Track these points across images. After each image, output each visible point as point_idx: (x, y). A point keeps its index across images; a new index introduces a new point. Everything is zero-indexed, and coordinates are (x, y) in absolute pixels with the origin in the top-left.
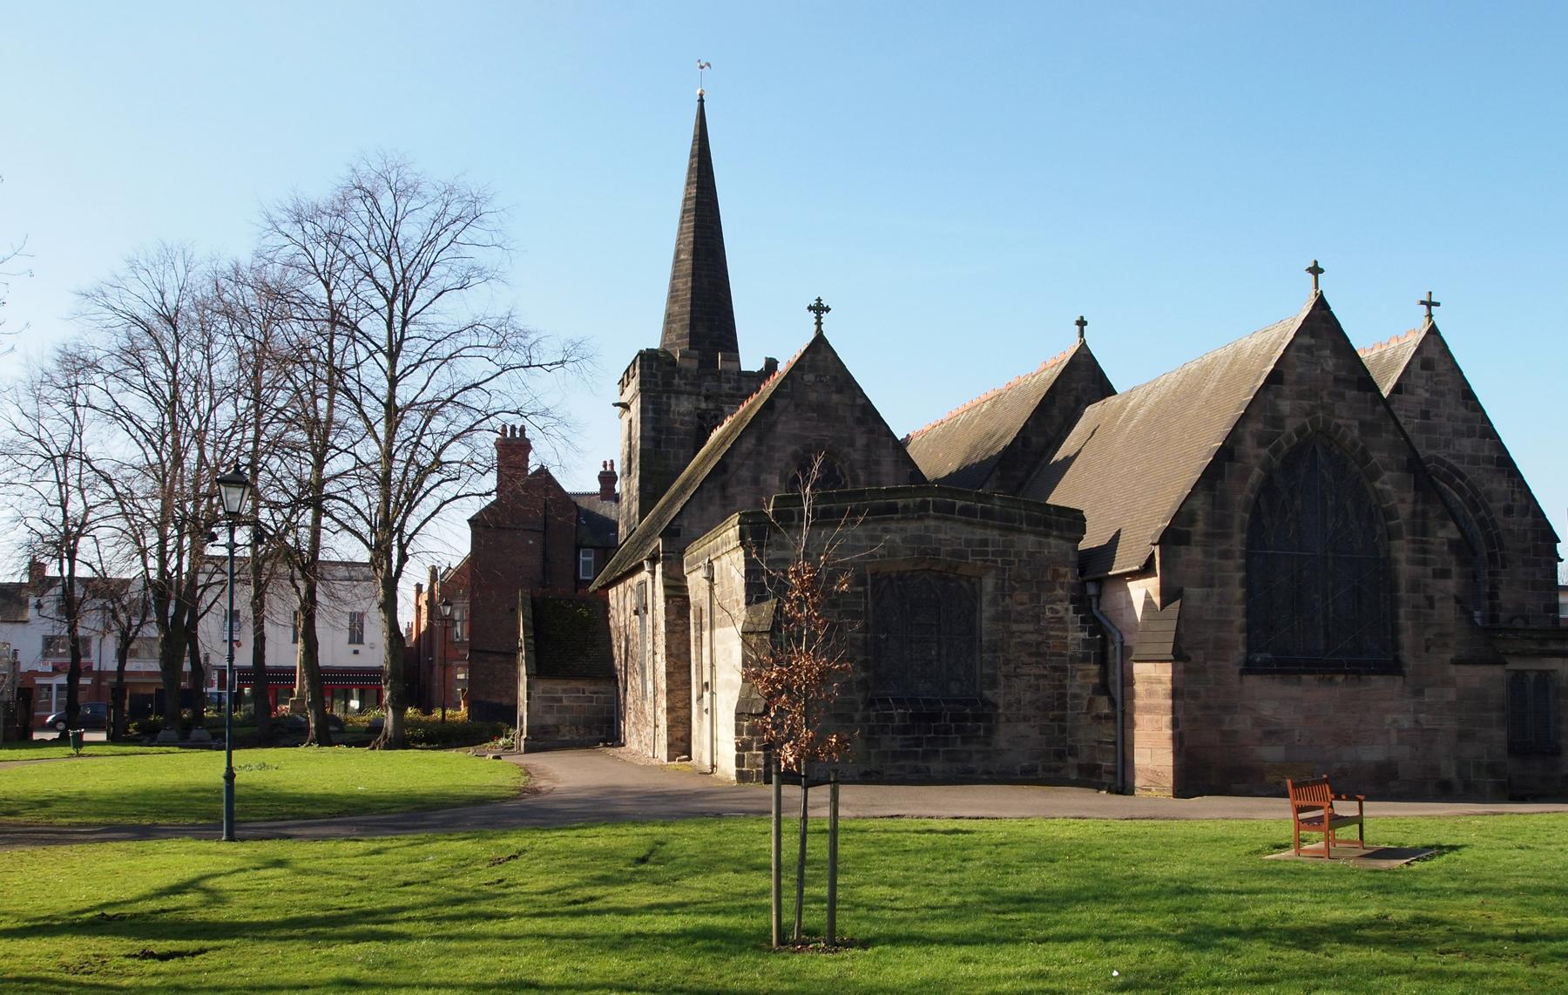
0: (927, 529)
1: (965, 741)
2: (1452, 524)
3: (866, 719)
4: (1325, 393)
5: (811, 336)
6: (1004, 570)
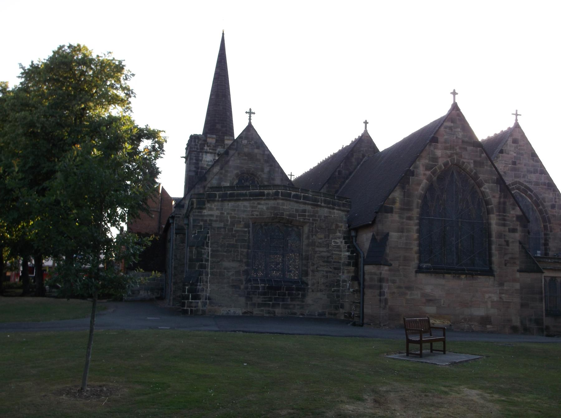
0: (278, 204)
1: (292, 300)
2: (518, 208)
3: (246, 288)
4: (457, 148)
5: (247, 124)
6: (313, 224)
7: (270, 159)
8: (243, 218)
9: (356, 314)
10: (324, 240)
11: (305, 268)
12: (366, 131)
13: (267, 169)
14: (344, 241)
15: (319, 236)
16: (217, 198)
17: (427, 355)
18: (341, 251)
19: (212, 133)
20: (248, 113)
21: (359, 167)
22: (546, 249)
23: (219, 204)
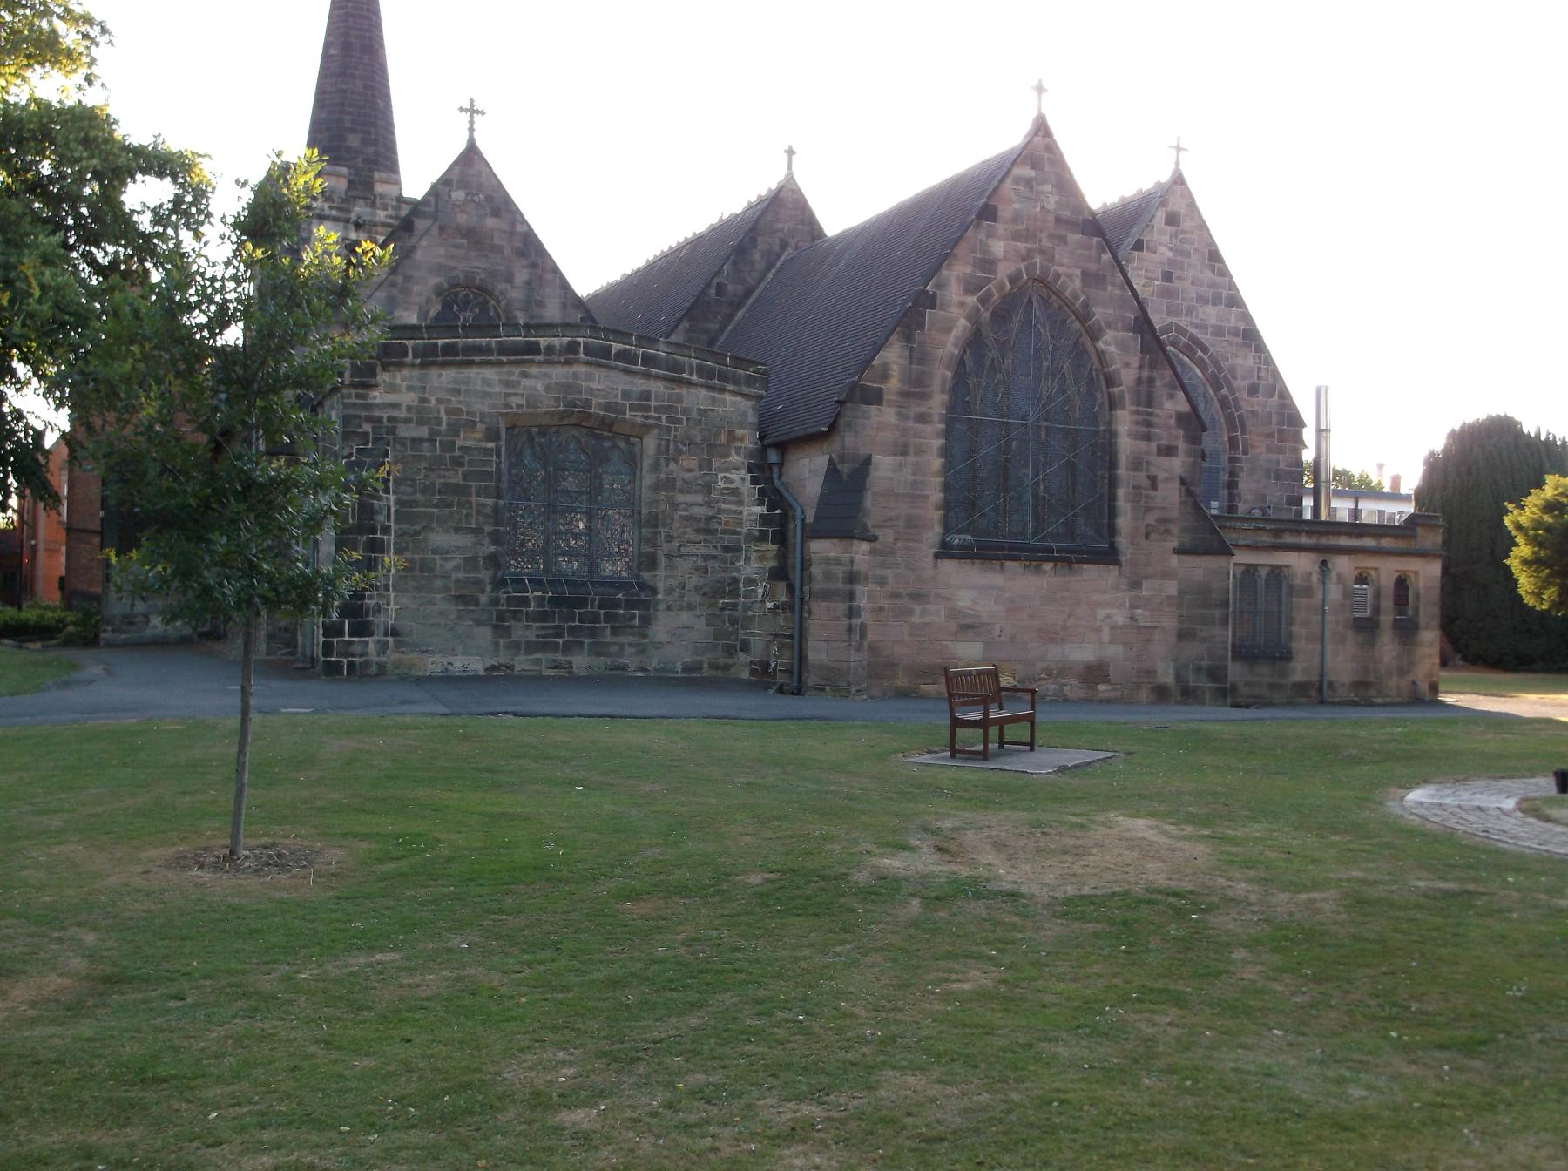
1: (616, 631)
3: (495, 602)
5: (463, 146)
6: (669, 430)
7: (530, 248)
10: (697, 473)
11: (648, 549)
13: (521, 276)
15: (685, 464)
17: (997, 755)
18: (740, 503)
20: (478, 112)
22: (1231, 498)
23: (416, 373)
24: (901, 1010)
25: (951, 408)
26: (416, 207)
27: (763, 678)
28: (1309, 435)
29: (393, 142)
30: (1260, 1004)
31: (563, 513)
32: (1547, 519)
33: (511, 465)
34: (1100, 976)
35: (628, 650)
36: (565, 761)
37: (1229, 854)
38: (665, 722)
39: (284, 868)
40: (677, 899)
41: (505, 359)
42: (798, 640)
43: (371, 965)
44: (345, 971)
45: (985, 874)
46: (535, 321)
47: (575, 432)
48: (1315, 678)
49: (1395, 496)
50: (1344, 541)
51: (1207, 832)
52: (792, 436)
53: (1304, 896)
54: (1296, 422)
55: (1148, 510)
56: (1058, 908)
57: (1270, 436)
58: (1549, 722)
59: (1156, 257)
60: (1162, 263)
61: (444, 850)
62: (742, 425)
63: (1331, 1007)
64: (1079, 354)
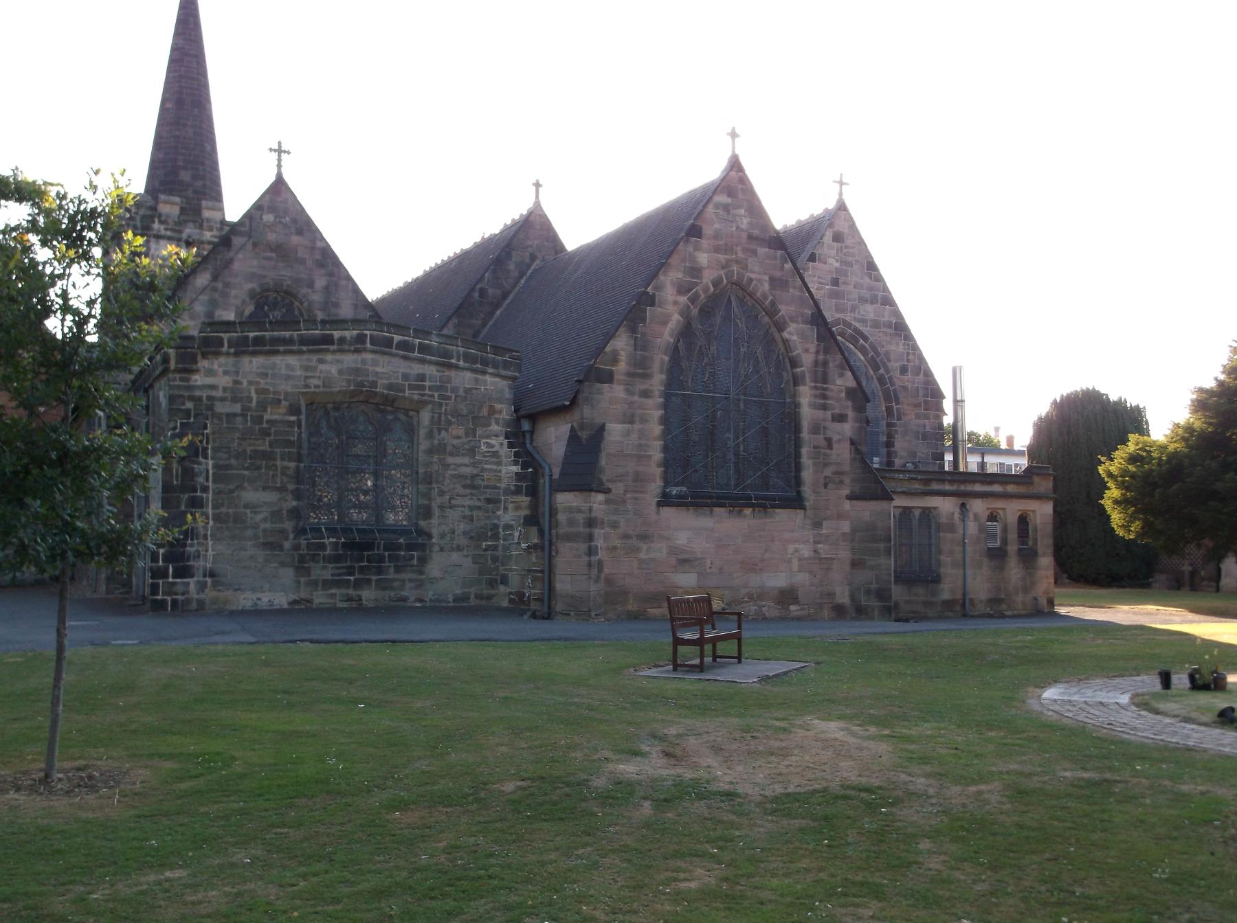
1: (398, 570)
2: (849, 374)
3: (297, 547)
4: (739, 249)
5: (272, 179)
6: (440, 405)
7: (328, 260)
8: (286, 394)
9: (535, 594)
10: (464, 440)
12: (537, 204)
13: (320, 283)
14: (506, 442)
15: (454, 432)
16: (225, 349)
17: (712, 667)
19: (170, 192)
21: (523, 281)
22: (889, 454)
23: (231, 360)
24: (636, 912)
25: (669, 384)
26: (234, 227)
27: (519, 606)
28: (948, 405)
29: (218, 177)
30: (948, 894)
31: (354, 473)
32: (1132, 468)
33: (311, 435)
34: (807, 870)
35: (408, 585)
36: (351, 682)
37: (907, 751)
38: (438, 645)
39: (93, 789)
40: (440, 808)
41: (305, 348)
42: (548, 574)
43: (159, 883)
44: (135, 889)
45: (706, 776)
46: (332, 318)
47: (363, 407)
48: (959, 596)
49: (1010, 452)
50: (978, 488)
51: (887, 732)
52: (541, 409)
53: (973, 789)
54: (937, 395)
55: (826, 465)
56: (769, 806)
57: (918, 405)
58: (1142, 628)
59: (826, 267)
60: (830, 272)
61: (238, 767)
62: (500, 401)
63: (1008, 894)
64: (769, 342)
